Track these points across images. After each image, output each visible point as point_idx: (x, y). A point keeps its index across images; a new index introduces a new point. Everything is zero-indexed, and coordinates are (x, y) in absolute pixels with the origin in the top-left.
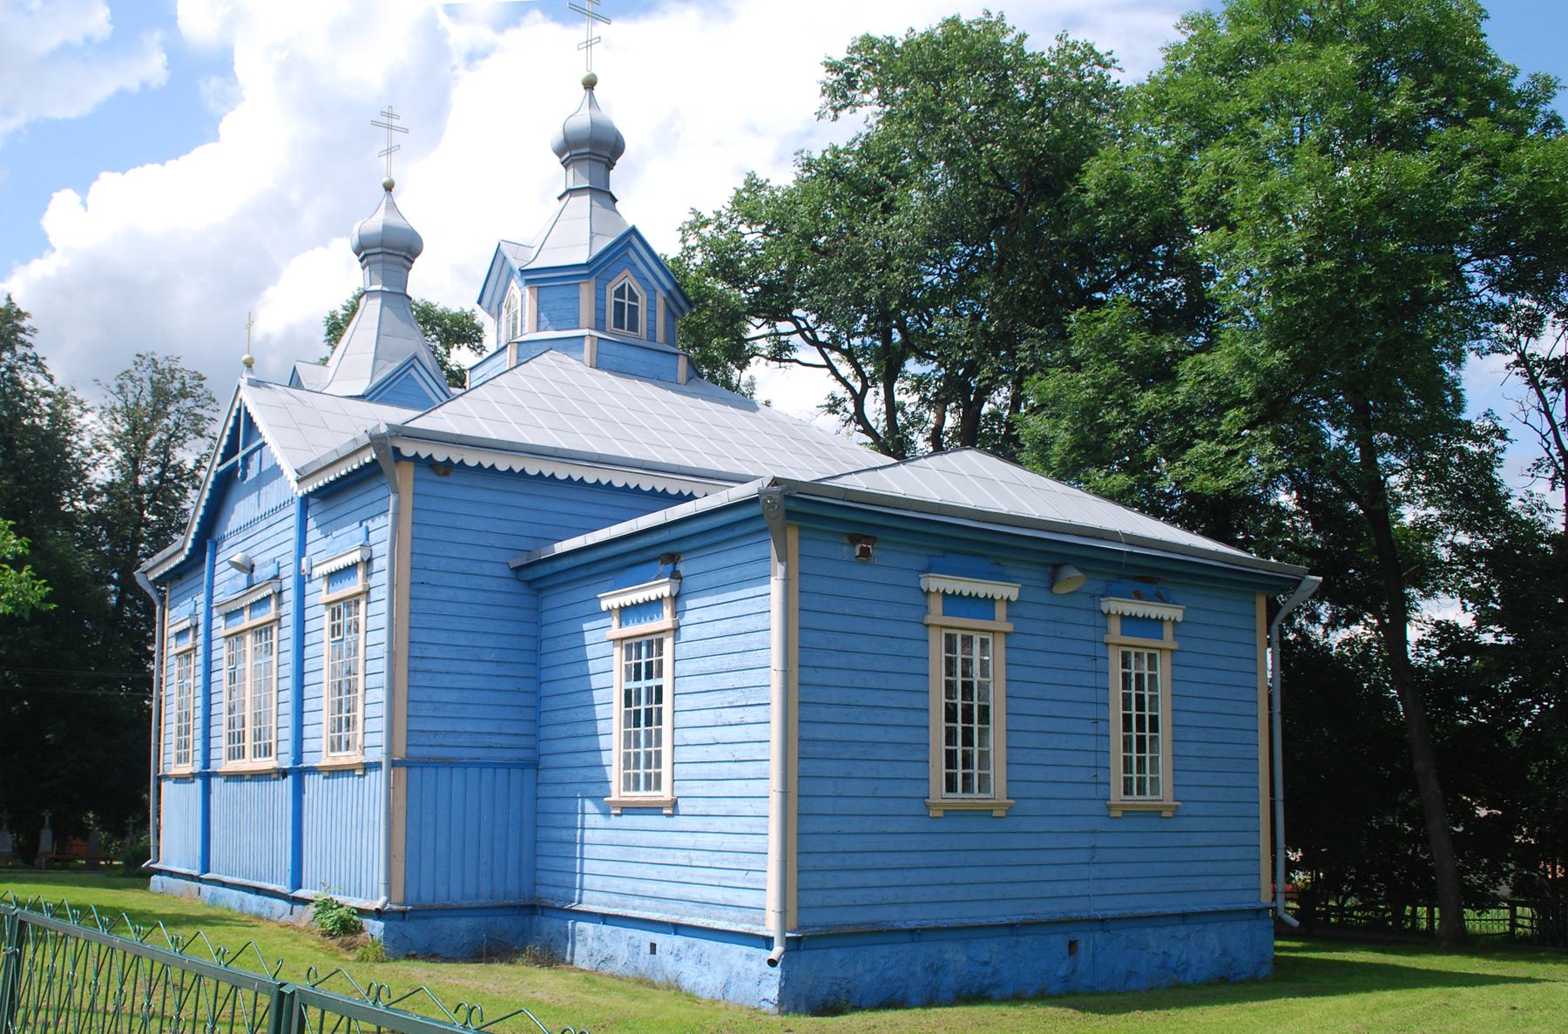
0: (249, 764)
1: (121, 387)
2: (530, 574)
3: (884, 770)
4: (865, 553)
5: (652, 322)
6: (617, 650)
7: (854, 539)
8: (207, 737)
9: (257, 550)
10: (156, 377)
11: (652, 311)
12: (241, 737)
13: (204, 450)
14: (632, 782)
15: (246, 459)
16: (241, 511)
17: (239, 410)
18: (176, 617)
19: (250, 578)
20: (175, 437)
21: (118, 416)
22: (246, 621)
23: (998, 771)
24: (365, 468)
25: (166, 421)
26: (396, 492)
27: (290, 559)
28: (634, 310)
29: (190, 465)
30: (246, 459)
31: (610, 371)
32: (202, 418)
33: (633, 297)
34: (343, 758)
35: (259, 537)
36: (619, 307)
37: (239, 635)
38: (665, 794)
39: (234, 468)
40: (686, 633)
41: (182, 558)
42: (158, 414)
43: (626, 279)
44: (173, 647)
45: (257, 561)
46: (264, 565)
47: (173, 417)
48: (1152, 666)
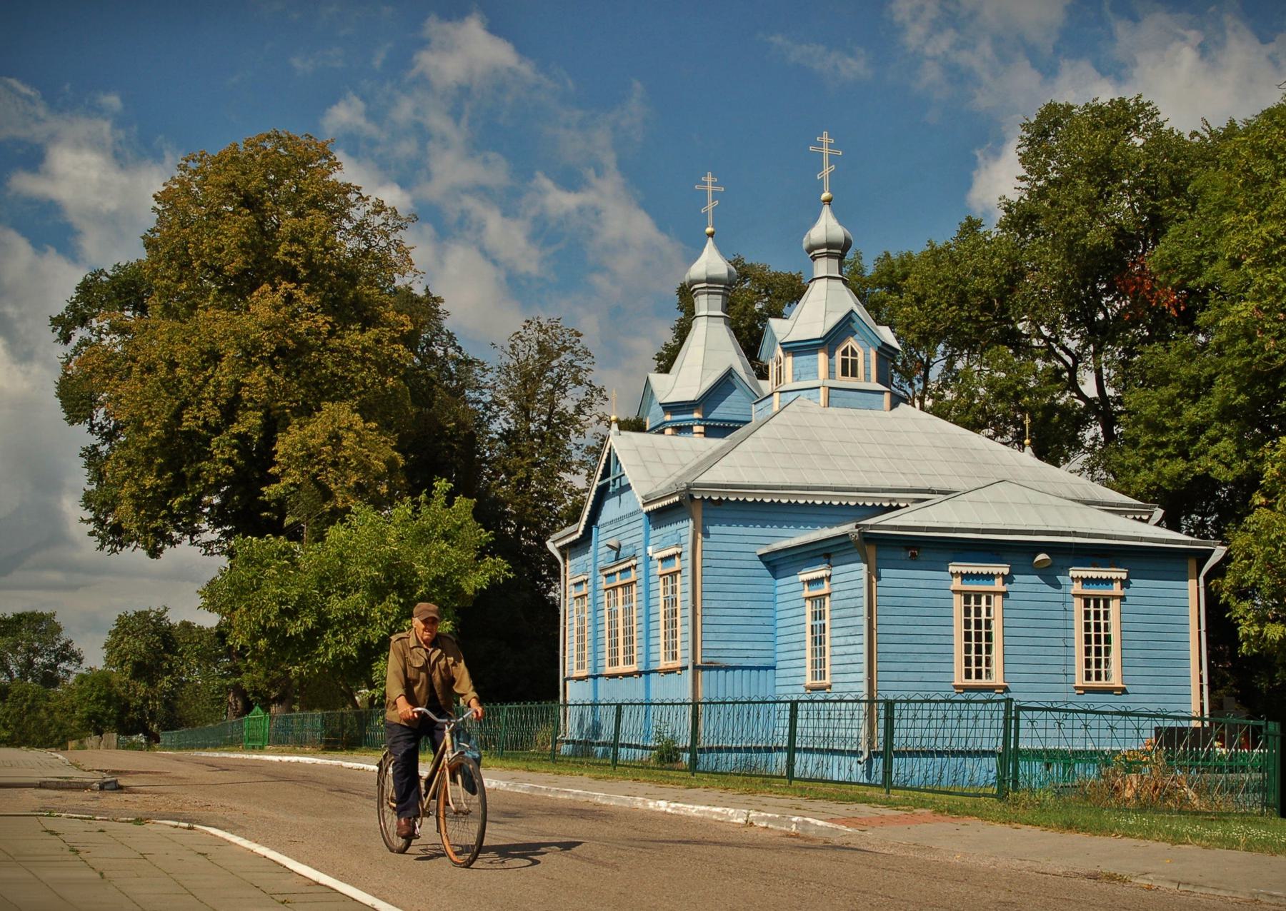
0: (622, 668)
1: (512, 347)
2: (767, 559)
3: (927, 667)
4: (913, 555)
5: (866, 368)
6: (808, 603)
7: (908, 549)
8: (595, 652)
9: (623, 536)
10: (542, 337)
11: (866, 361)
12: (617, 652)
13: (583, 397)
14: (814, 677)
15: (614, 480)
16: (611, 509)
17: (609, 454)
18: (572, 569)
19: (618, 554)
20: (559, 386)
21: (512, 374)
22: (618, 580)
23: (997, 666)
24: (675, 503)
25: (549, 374)
26: (693, 518)
27: (640, 546)
28: (855, 363)
29: (571, 410)
30: (614, 480)
31: (337, 892)
32: (580, 370)
33: (854, 353)
34: (671, 664)
35: (624, 529)
36: (844, 362)
37: (614, 588)
38: (827, 681)
39: (607, 485)
40: (835, 596)
41: (577, 536)
42: (545, 368)
43: (851, 343)
44: (573, 592)
45: (624, 543)
46: (627, 547)
47: (556, 370)
48: (1106, 605)
